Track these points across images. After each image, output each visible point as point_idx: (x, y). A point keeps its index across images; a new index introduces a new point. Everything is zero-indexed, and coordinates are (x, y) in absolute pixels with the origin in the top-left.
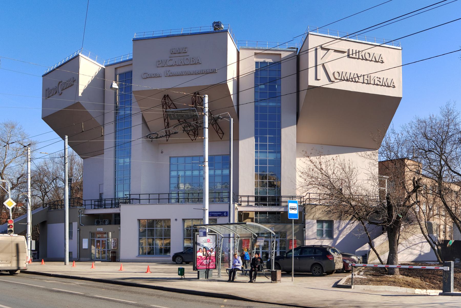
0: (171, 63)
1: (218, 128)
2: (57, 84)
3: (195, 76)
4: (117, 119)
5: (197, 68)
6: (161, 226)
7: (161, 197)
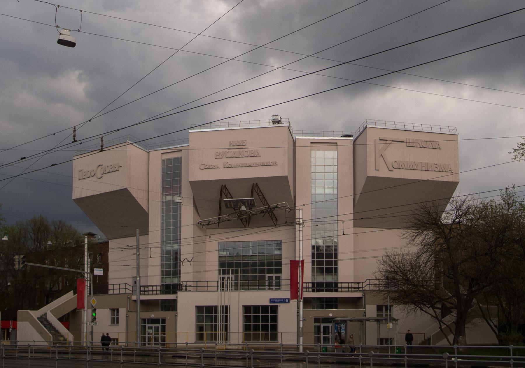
0: (229, 155)
1: (227, 192)
5: (257, 160)
6: (70, 243)
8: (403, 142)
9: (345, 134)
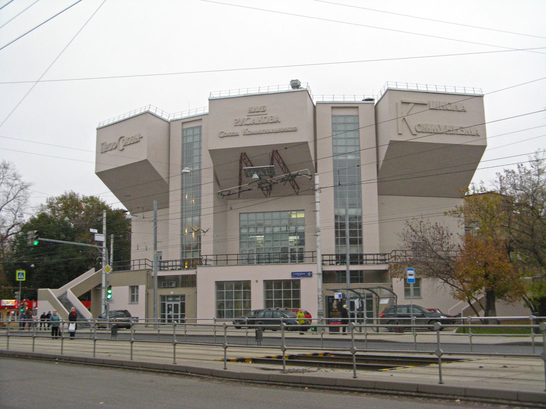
0: (248, 122)
2: (118, 138)
3: (429, 134)
4: (184, 210)
5: (276, 127)
7: (219, 258)
8: (426, 104)
9: (366, 97)
